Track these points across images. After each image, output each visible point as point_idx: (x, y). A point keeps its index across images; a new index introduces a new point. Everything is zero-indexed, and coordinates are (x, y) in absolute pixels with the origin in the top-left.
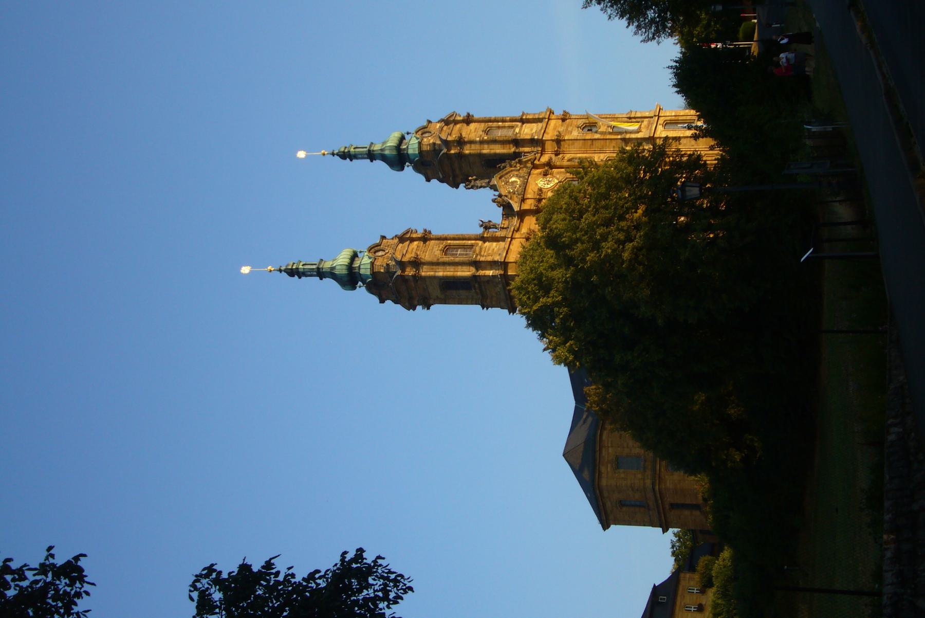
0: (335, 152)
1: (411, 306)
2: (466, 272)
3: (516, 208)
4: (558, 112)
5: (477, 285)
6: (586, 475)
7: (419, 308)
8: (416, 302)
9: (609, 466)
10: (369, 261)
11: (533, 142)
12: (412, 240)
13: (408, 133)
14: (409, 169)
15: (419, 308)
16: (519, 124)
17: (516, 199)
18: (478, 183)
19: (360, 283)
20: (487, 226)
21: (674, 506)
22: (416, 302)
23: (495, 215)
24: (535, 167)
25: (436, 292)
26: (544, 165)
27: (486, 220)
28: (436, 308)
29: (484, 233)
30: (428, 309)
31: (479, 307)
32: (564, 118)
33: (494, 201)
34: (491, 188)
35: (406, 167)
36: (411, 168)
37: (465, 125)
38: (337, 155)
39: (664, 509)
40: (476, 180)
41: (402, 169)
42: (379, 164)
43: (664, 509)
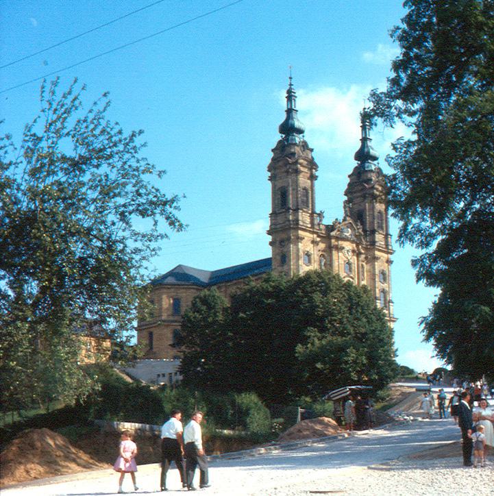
0: (292, 87)
1: (270, 168)
2: (291, 204)
3: (333, 233)
4: (392, 257)
5: (284, 210)
6: (170, 280)
7: (269, 174)
8: (350, 196)
9: (175, 294)
10: (297, 142)
11: (373, 243)
12: (311, 169)
13: (303, 136)
14: (355, 163)
15: (269, 174)
16: (310, 212)
17: (338, 233)
18: (347, 209)
19: (284, 136)
20: (320, 215)
21: (151, 334)
22: (350, 196)
23: (328, 221)
24: (357, 246)
25: (279, 184)
26: (358, 249)
27: (324, 214)
28: (269, 185)
29: (316, 214)
30: (269, 180)
31: (271, 212)
32: (389, 262)
33: (337, 219)
34: (345, 217)
35: (357, 162)
36: (357, 165)
37: (308, 175)
38: (290, 88)
39: (150, 328)
40: (349, 207)
41: (356, 159)
42: (283, 117)
43: (150, 328)
